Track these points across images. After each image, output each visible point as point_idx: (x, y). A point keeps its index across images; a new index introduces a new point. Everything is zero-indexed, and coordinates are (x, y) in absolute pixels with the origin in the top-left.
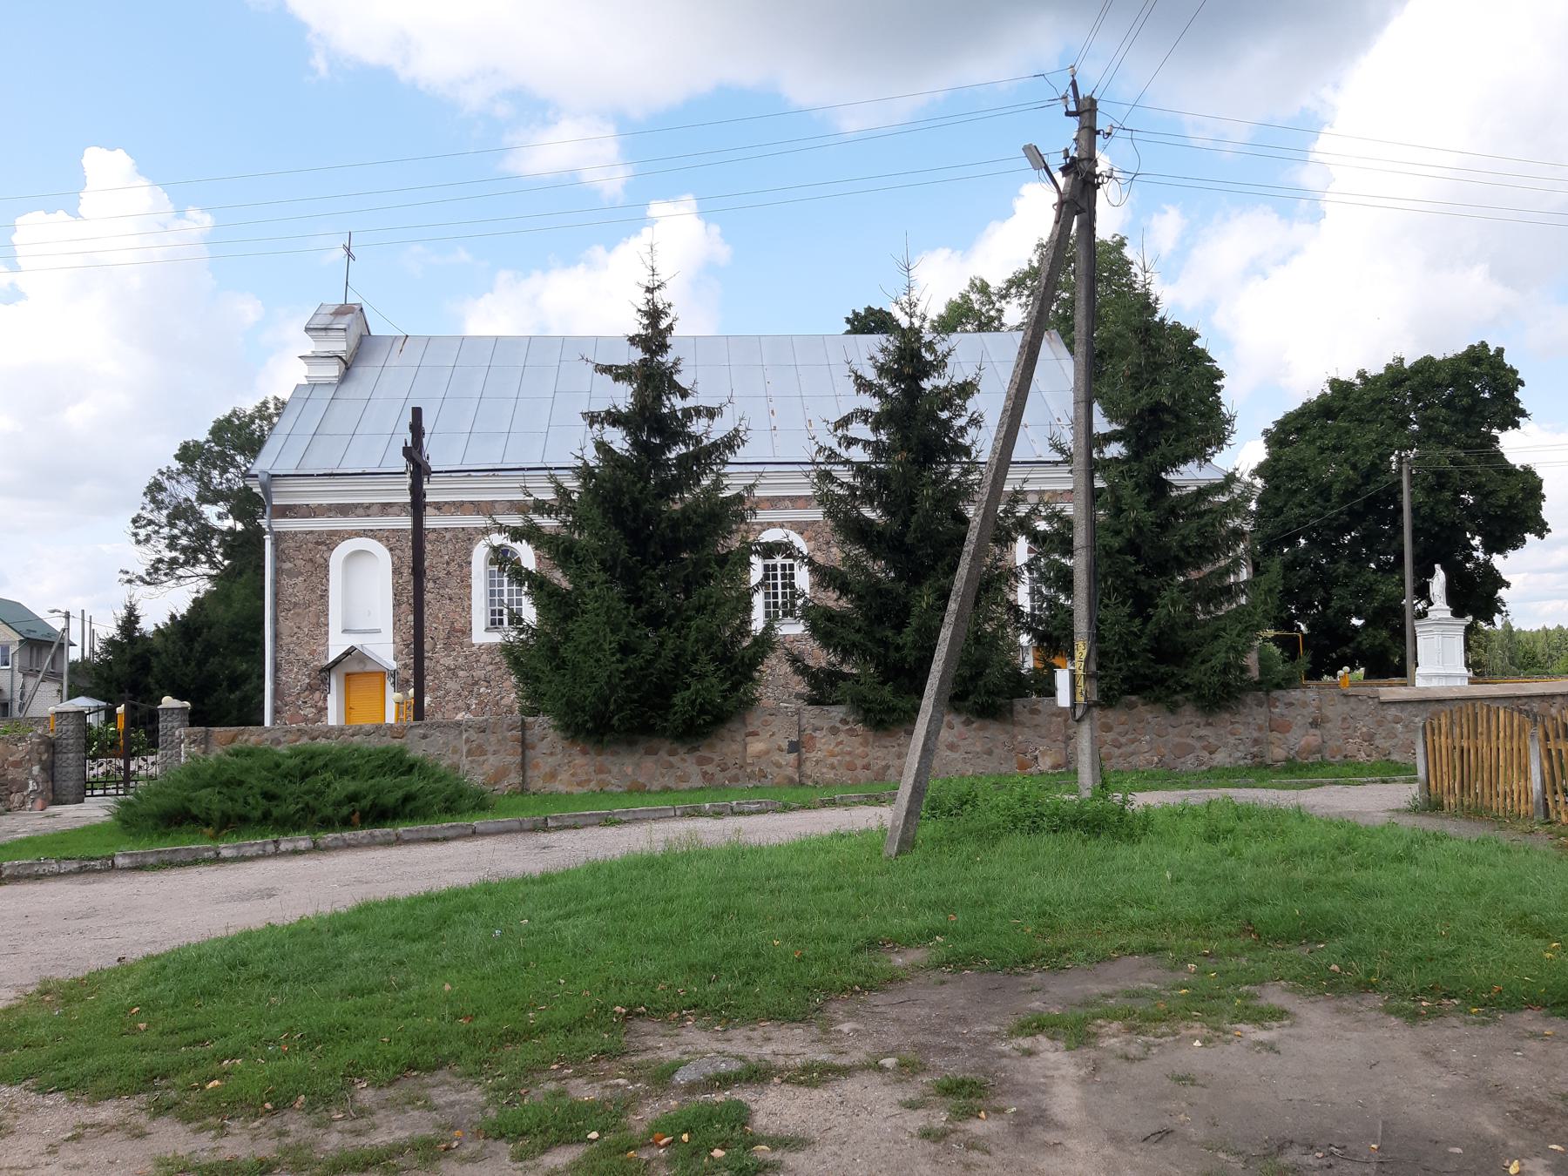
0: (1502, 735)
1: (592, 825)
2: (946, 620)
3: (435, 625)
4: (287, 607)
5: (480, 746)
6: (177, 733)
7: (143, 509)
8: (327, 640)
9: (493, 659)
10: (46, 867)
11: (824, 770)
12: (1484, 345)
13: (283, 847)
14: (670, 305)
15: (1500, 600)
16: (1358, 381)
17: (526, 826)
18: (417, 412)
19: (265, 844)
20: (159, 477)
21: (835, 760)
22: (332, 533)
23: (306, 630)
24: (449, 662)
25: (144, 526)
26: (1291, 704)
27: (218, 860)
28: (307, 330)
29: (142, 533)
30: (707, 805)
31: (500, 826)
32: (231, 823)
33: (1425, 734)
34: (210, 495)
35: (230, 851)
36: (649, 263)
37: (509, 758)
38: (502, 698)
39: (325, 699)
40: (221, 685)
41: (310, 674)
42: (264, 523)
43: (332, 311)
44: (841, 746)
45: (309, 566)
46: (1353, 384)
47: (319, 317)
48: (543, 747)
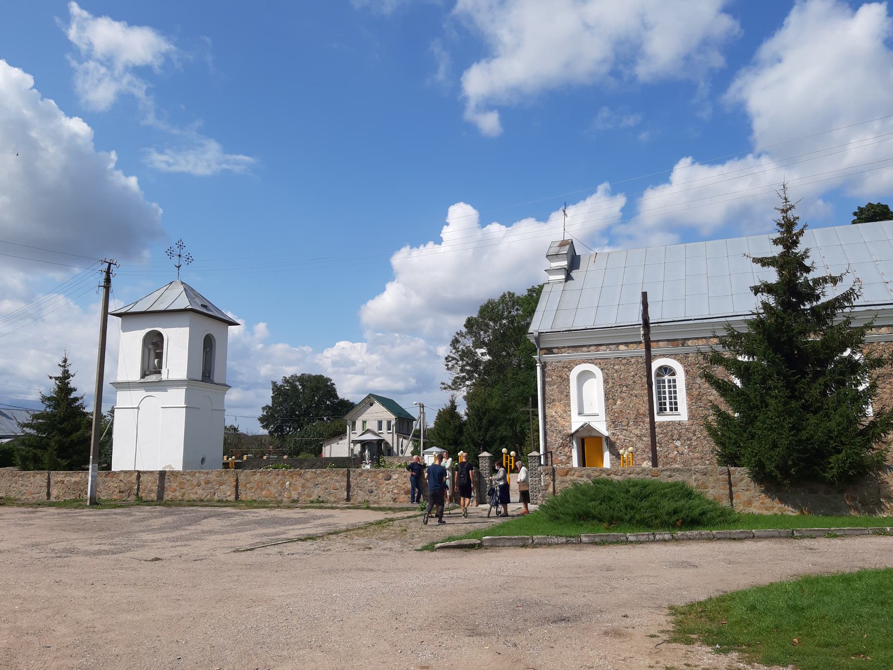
1: (820, 536)
3: (628, 411)
4: (549, 401)
5: (703, 483)
6: (539, 469)
7: (451, 352)
8: (571, 419)
9: (663, 431)
13: (658, 537)
14: (797, 218)
18: (645, 295)
20: (457, 336)
22: (570, 362)
24: (637, 432)
25: (450, 361)
27: (627, 542)
28: (547, 256)
29: (450, 364)
31: (768, 533)
34: (479, 344)
35: (633, 537)
37: (722, 491)
38: (669, 454)
42: (536, 357)
48: (742, 485)
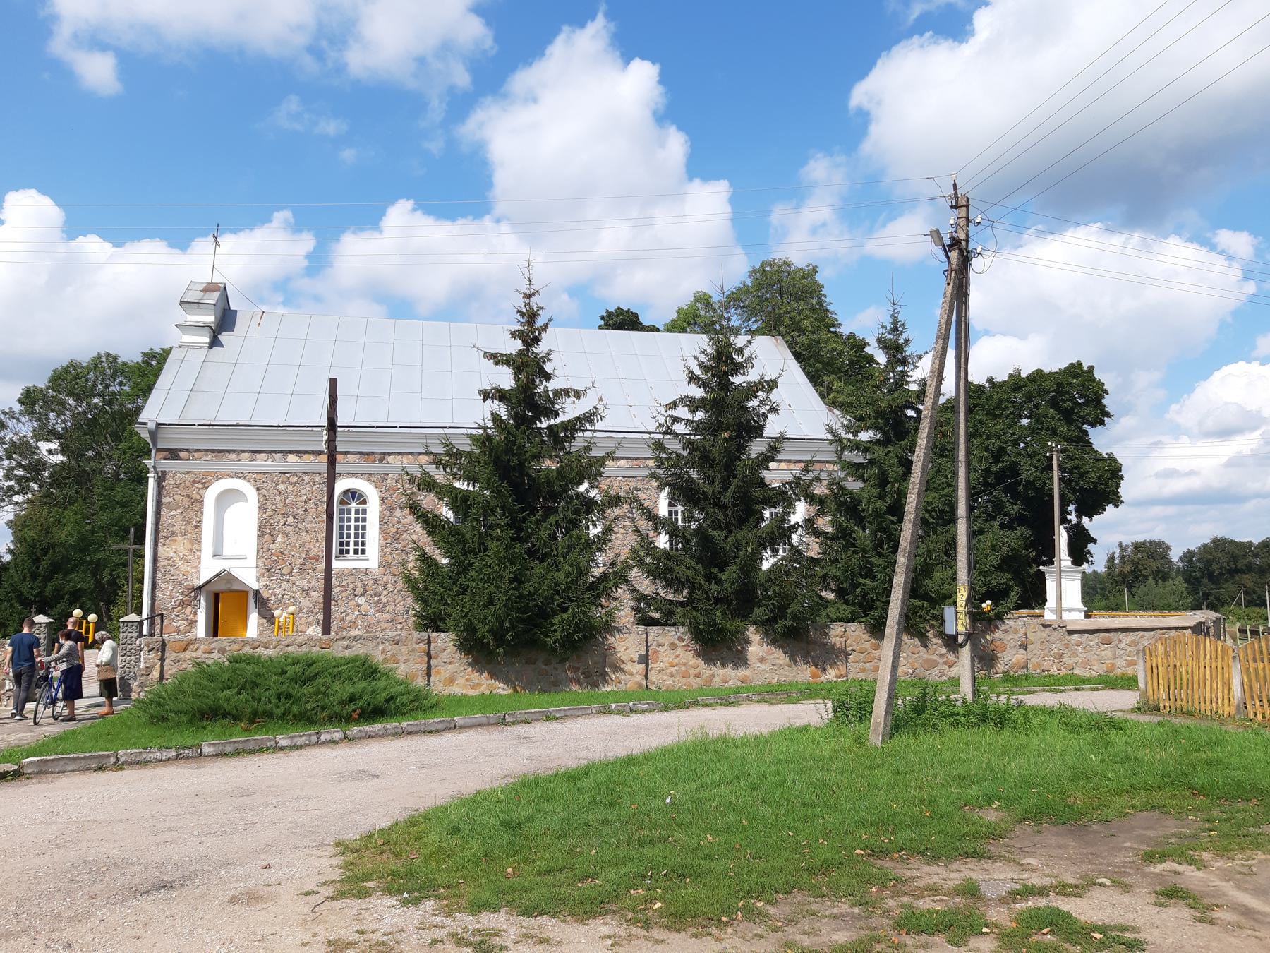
0: (1208, 657)
2: (897, 570)
4: (165, 534)
5: (393, 655)
10: (151, 755)
11: (665, 678)
12: (1080, 364)
13: (323, 738)
14: (542, 308)
15: (1089, 552)
16: (987, 385)
17: (491, 721)
18: (333, 382)
19: (310, 735)
21: (673, 670)
23: (181, 554)
24: (304, 584)
26: (1006, 631)
27: (277, 748)
28: (181, 303)
30: (613, 706)
31: (474, 721)
32: (258, 718)
33: (1145, 654)
35: (285, 741)
36: (527, 275)
37: (417, 666)
38: (346, 616)
39: (195, 614)
40: (63, 599)
41: (183, 593)
42: (149, 463)
43: (201, 288)
44: (678, 659)
45: (186, 501)
46: (984, 387)
47: (190, 293)
48: (444, 656)
